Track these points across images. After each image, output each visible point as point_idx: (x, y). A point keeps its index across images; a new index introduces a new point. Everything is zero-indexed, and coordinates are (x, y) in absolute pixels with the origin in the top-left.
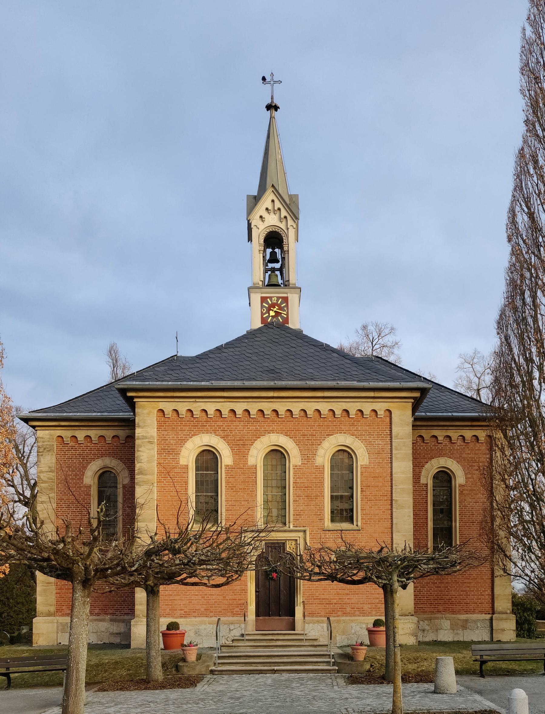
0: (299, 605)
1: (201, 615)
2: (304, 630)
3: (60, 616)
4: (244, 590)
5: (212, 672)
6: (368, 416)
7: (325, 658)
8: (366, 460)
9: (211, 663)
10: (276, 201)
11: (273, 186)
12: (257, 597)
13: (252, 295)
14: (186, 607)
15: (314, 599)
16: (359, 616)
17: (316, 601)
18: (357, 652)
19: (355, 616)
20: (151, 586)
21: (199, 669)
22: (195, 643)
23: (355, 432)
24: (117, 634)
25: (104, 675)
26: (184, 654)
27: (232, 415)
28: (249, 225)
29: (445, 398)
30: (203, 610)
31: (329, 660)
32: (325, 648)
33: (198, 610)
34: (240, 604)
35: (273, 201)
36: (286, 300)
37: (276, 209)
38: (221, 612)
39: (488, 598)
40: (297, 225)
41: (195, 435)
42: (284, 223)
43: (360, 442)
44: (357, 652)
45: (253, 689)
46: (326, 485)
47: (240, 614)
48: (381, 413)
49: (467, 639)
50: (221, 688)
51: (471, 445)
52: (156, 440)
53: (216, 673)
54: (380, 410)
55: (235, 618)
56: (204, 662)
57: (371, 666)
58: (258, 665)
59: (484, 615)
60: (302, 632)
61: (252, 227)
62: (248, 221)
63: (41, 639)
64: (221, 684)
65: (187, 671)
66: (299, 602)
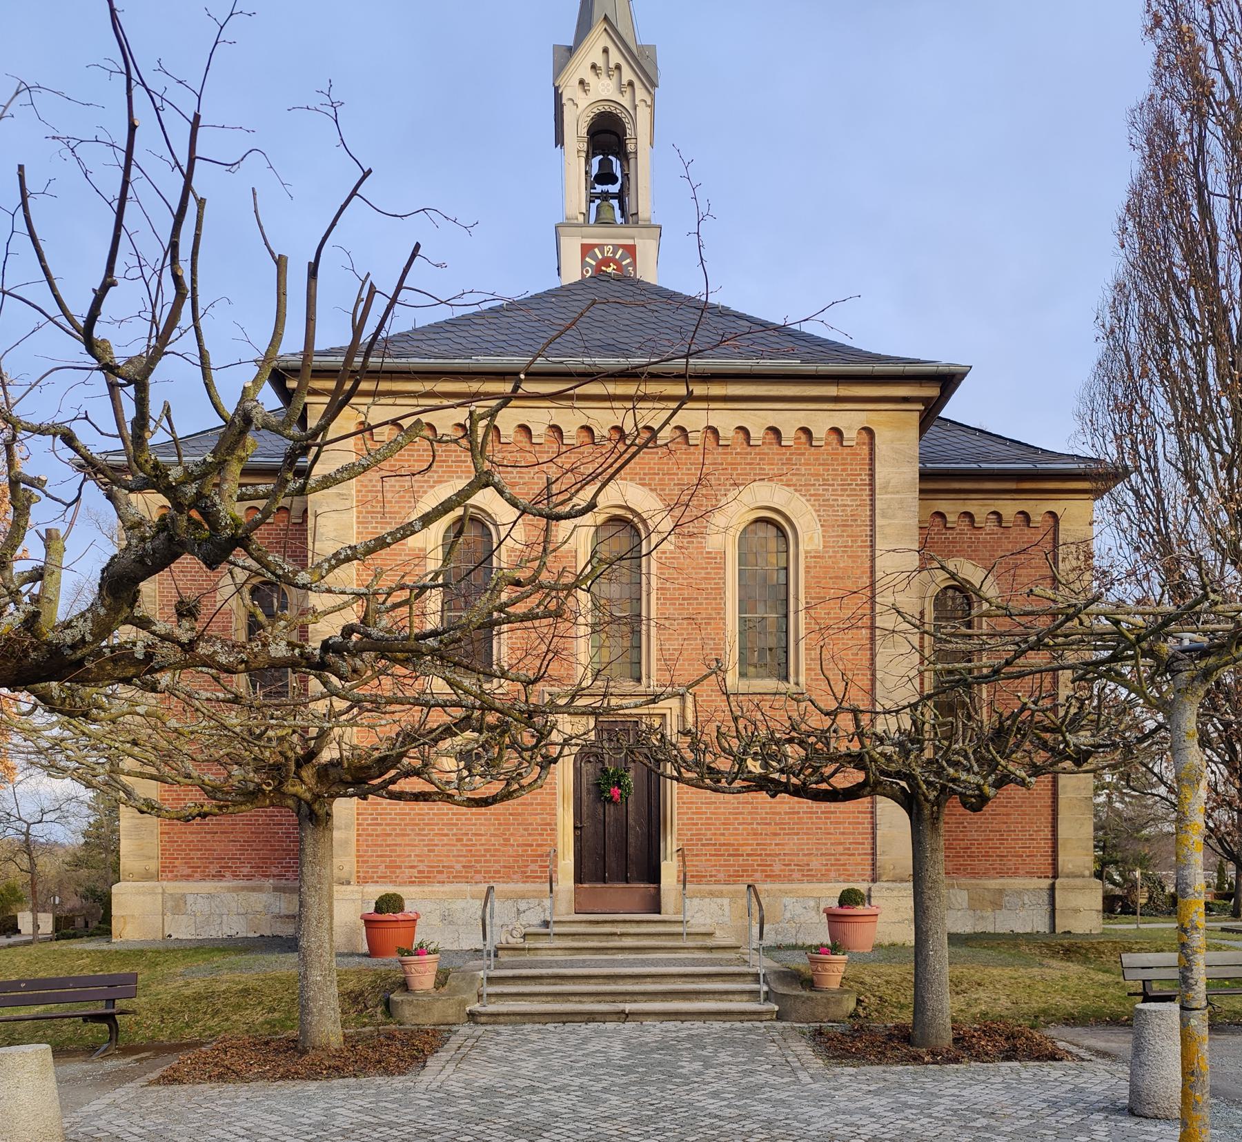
0: (669, 857)
1: (457, 878)
2: (682, 910)
3: (169, 880)
4: (549, 824)
5: (472, 1016)
6: (822, 443)
7: (744, 982)
8: (816, 541)
9: (471, 996)
10: (613, 52)
11: (606, 18)
12: (578, 839)
13: (563, 240)
14: (422, 861)
15: (703, 845)
16: (801, 881)
17: (705, 850)
18: (826, 970)
19: (791, 881)
20: (307, 802)
21: (443, 1010)
22: (432, 947)
23: (794, 478)
24: (288, 917)
25: (211, 1023)
26: (405, 972)
27: (522, 438)
28: (558, 97)
29: (955, 440)
30: (458, 867)
31: (755, 987)
32: (731, 955)
33: (448, 867)
34: (541, 856)
35: (606, 51)
36: (631, 250)
37: (612, 65)
38: (499, 872)
39: (1046, 846)
40: (653, 100)
41: (441, 482)
42: (628, 95)
43: (803, 499)
44: (826, 970)
45: (578, 1081)
46: (729, 594)
47: (540, 877)
48: (851, 435)
49: (1002, 928)
50: (486, 1076)
51: (1014, 532)
52: (354, 492)
53: (483, 1019)
54: (850, 428)
55: (530, 886)
56: (454, 992)
57: (859, 1002)
58: (585, 999)
59: (1036, 880)
60: (680, 917)
61: (564, 101)
62: (556, 89)
63: (129, 928)
64: (492, 1059)
65: (411, 1014)
66: (669, 851)
